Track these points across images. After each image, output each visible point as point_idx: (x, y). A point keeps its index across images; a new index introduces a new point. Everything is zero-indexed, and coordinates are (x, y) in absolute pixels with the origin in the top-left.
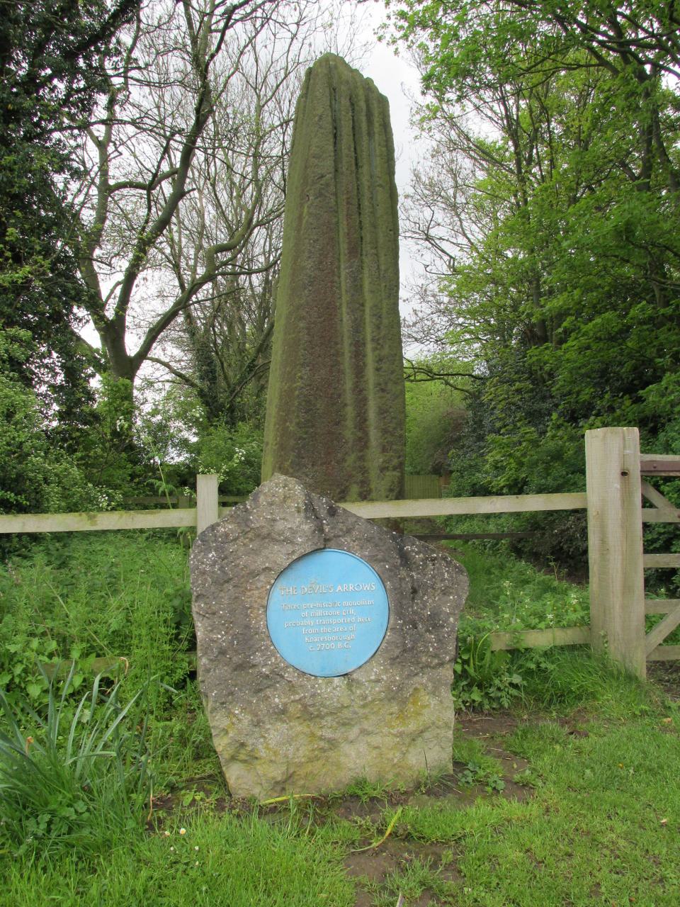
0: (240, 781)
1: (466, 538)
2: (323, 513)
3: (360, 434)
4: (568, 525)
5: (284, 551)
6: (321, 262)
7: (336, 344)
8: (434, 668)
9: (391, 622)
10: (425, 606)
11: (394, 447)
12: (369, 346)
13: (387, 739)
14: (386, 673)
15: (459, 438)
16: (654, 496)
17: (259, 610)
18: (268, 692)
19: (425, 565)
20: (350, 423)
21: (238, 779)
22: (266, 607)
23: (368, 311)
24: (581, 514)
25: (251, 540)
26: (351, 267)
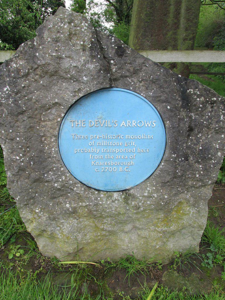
0: (46, 248)
1: (215, 74)
2: (111, 53)
3: (176, 21)
5: (71, 88)
8: (197, 188)
9: (166, 155)
10: (198, 142)
11: (192, 28)
13: (152, 234)
14: (157, 192)
15: (220, 32)
17: (51, 138)
18: (61, 199)
19: (205, 107)
20: (171, 15)
21: (44, 247)
22: (58, 137)
25: (41, 77)
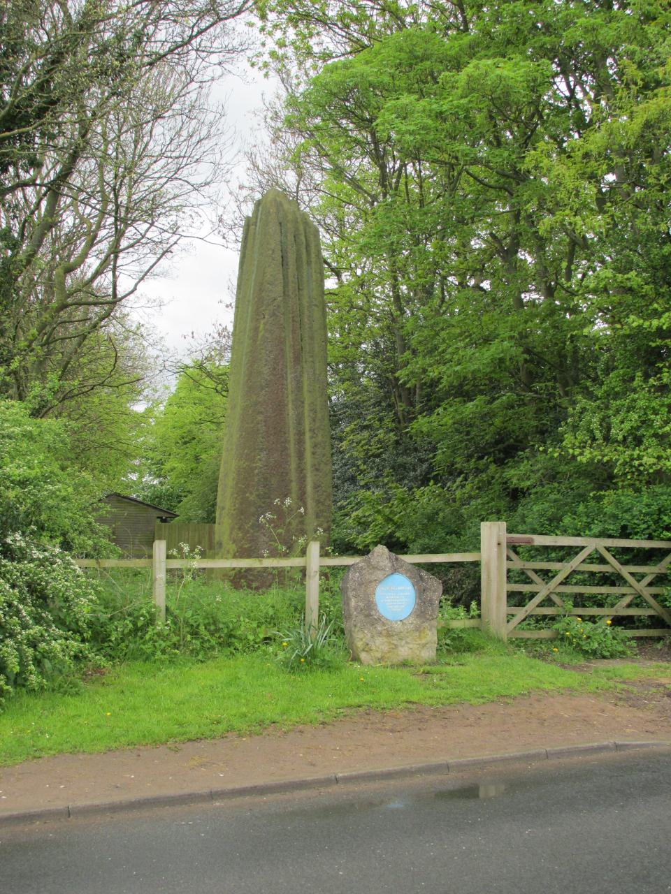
4: (449, 577)
6: (274, 369)
7: (285, 433)
12: (308, 435)
16: (513, 555)
23: (306, 406)
24: (476, 564)
26: (296, 372)
